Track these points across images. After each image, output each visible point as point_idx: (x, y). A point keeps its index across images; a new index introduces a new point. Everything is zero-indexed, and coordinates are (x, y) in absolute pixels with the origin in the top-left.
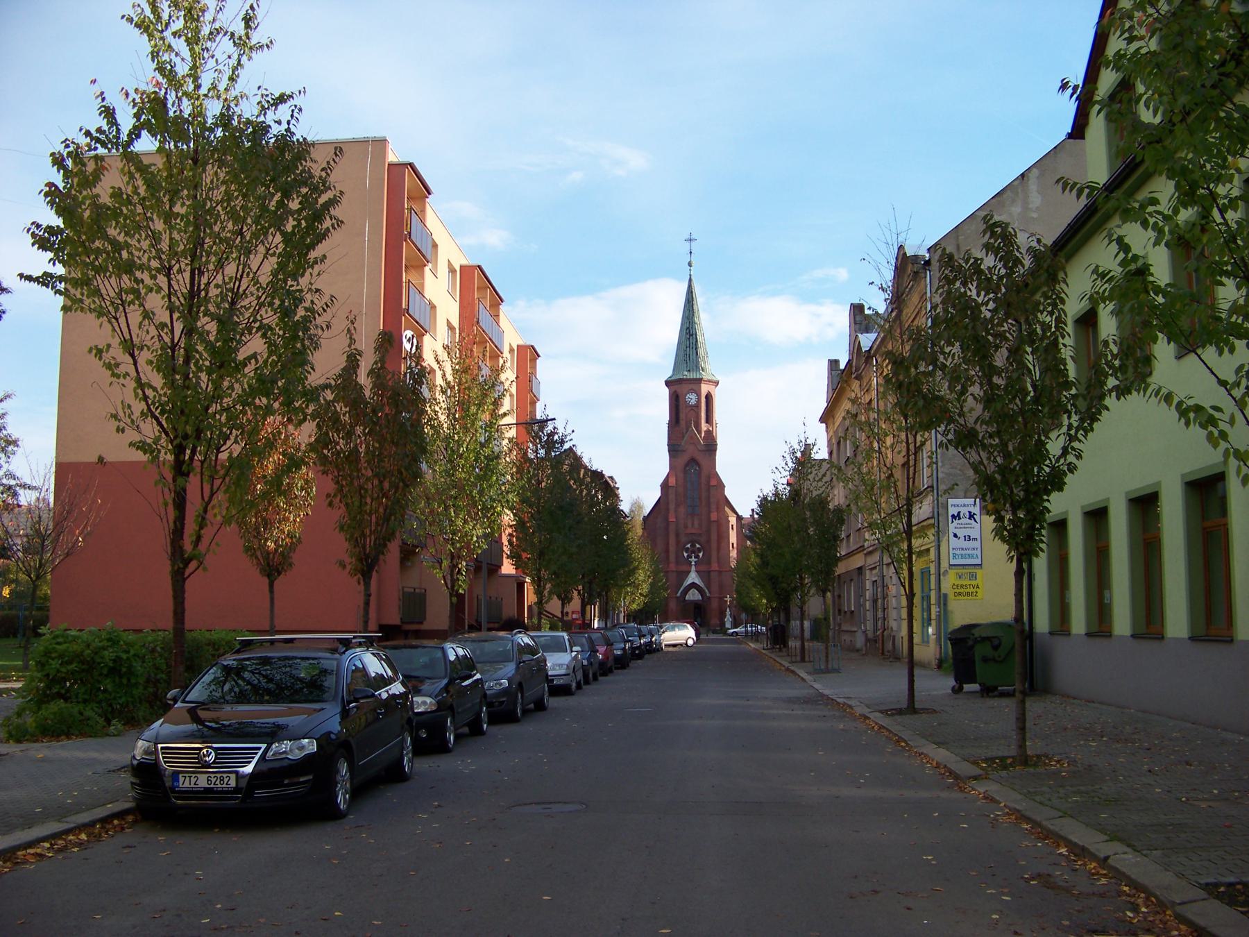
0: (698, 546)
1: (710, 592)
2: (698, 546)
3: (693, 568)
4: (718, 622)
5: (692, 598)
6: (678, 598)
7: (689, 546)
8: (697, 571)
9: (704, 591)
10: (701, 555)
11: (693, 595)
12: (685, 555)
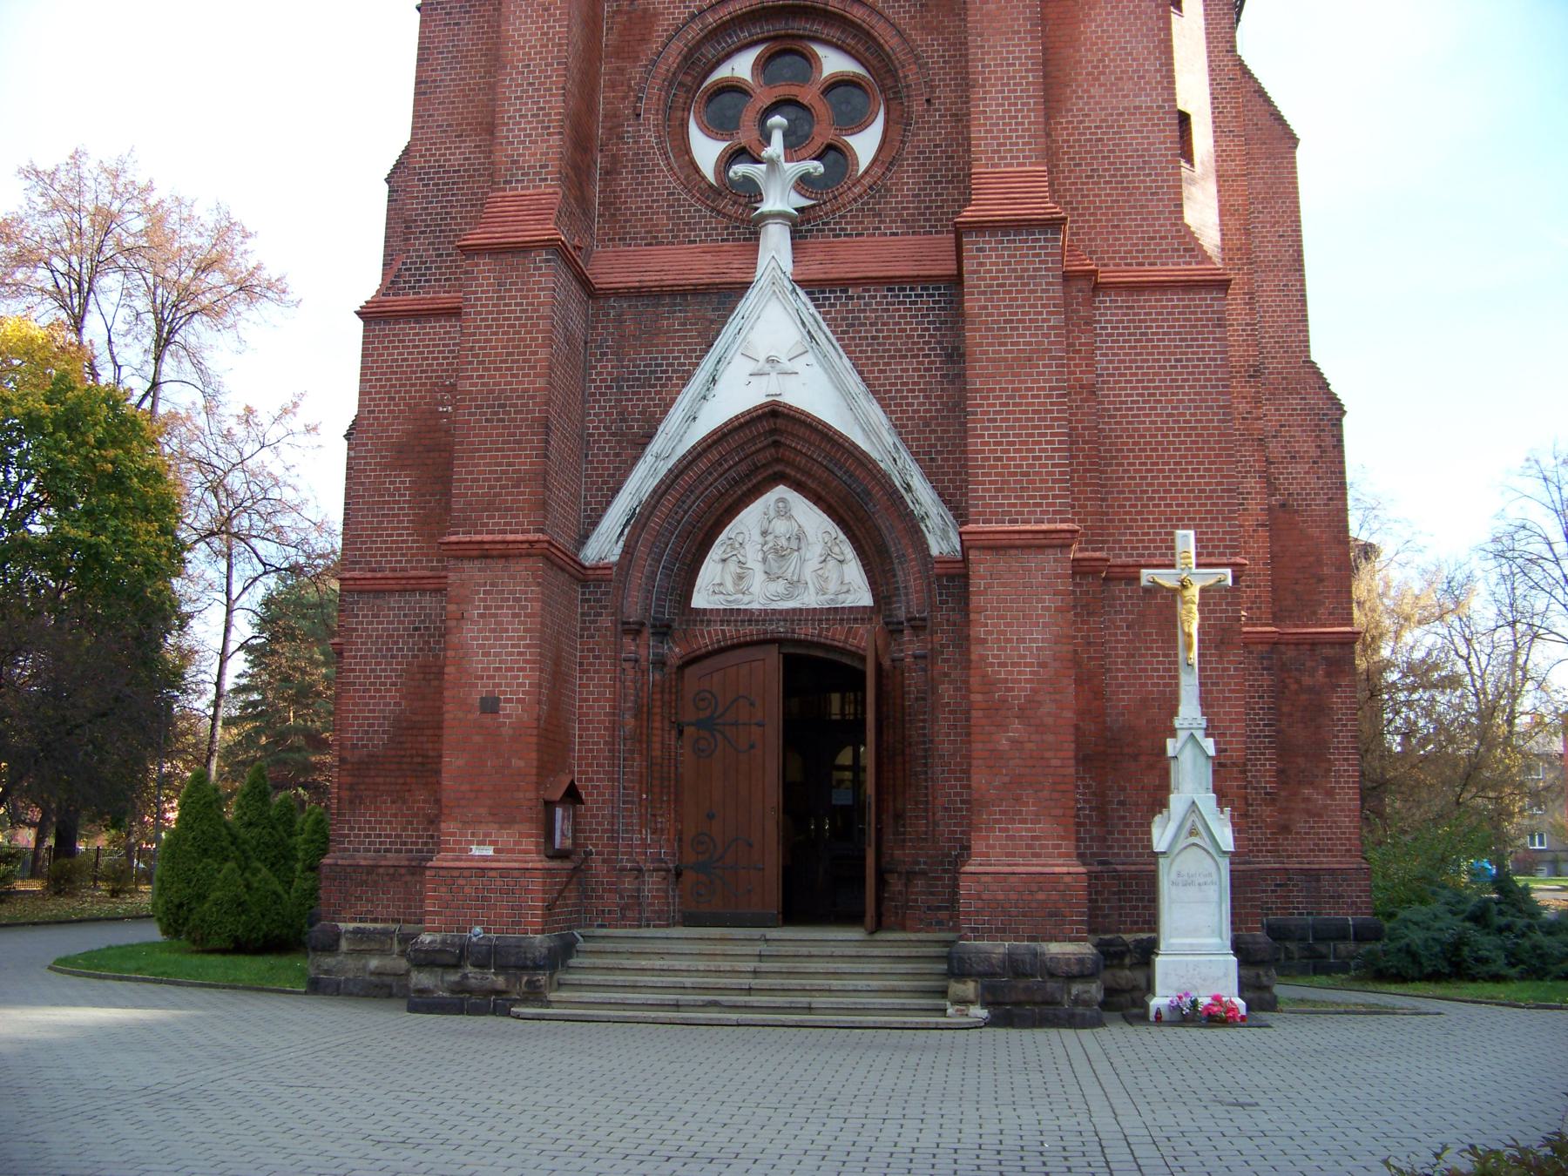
0: (833, 63)
1: (957, 505)
2: (833, 63)
3: (776, 246)
4: (1066, 866)
5: (760, 594)
6: (586, 577)
7: (742, 67)
8: (814, 287)
9: (895, 500)
10: (865, 145)
11: (779, 554)
12: (706, 151)
